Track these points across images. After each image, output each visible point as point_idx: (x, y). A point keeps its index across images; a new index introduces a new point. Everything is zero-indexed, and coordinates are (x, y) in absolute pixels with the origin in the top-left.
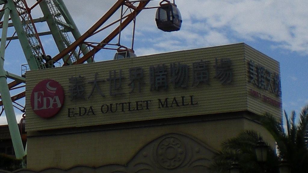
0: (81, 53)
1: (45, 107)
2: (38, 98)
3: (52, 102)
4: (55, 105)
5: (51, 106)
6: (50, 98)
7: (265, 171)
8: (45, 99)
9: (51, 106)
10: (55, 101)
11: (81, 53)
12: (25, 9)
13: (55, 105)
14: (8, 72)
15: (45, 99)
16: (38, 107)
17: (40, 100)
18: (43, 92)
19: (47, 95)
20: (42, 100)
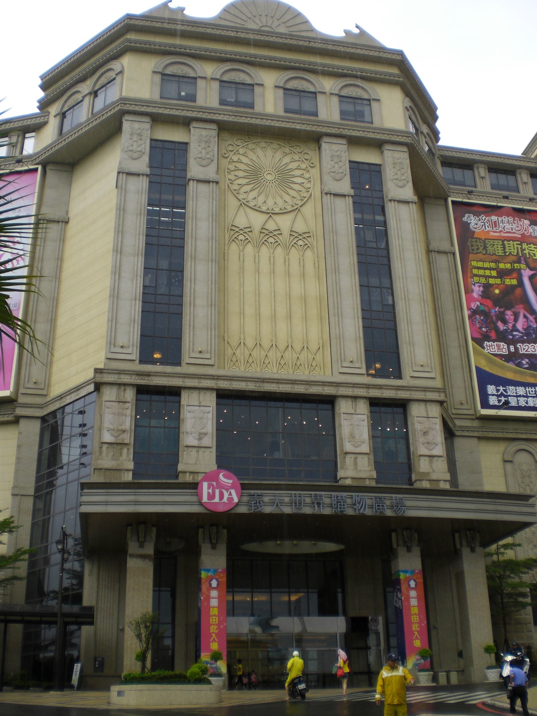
0: (24, 560)
1: (217, 500)
2: (209, 488)
3: (226, 495)
4: (230, 499)
5: (225, 500)
6: (224, 492)
7: (497, 291)
8: (217, 492)
9: (225, 500)
10: (230, 494)
11: (24, 560)
12: (236, 194)
13: (230, 499)
14: (57, 480)
15: (217, 492)
16: (209, 499)
17: (210, 491)
18: (215, 483)
19: (220, 486)
20: (214, 493)
